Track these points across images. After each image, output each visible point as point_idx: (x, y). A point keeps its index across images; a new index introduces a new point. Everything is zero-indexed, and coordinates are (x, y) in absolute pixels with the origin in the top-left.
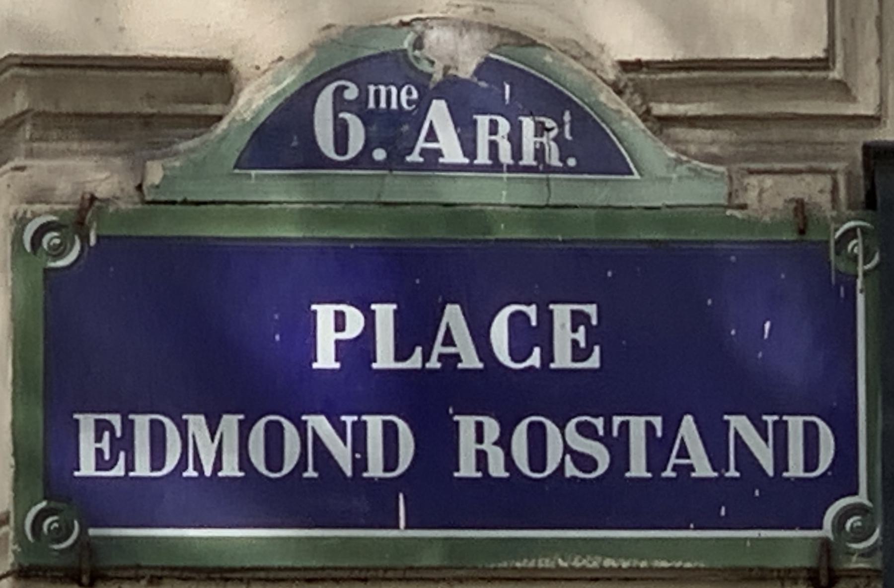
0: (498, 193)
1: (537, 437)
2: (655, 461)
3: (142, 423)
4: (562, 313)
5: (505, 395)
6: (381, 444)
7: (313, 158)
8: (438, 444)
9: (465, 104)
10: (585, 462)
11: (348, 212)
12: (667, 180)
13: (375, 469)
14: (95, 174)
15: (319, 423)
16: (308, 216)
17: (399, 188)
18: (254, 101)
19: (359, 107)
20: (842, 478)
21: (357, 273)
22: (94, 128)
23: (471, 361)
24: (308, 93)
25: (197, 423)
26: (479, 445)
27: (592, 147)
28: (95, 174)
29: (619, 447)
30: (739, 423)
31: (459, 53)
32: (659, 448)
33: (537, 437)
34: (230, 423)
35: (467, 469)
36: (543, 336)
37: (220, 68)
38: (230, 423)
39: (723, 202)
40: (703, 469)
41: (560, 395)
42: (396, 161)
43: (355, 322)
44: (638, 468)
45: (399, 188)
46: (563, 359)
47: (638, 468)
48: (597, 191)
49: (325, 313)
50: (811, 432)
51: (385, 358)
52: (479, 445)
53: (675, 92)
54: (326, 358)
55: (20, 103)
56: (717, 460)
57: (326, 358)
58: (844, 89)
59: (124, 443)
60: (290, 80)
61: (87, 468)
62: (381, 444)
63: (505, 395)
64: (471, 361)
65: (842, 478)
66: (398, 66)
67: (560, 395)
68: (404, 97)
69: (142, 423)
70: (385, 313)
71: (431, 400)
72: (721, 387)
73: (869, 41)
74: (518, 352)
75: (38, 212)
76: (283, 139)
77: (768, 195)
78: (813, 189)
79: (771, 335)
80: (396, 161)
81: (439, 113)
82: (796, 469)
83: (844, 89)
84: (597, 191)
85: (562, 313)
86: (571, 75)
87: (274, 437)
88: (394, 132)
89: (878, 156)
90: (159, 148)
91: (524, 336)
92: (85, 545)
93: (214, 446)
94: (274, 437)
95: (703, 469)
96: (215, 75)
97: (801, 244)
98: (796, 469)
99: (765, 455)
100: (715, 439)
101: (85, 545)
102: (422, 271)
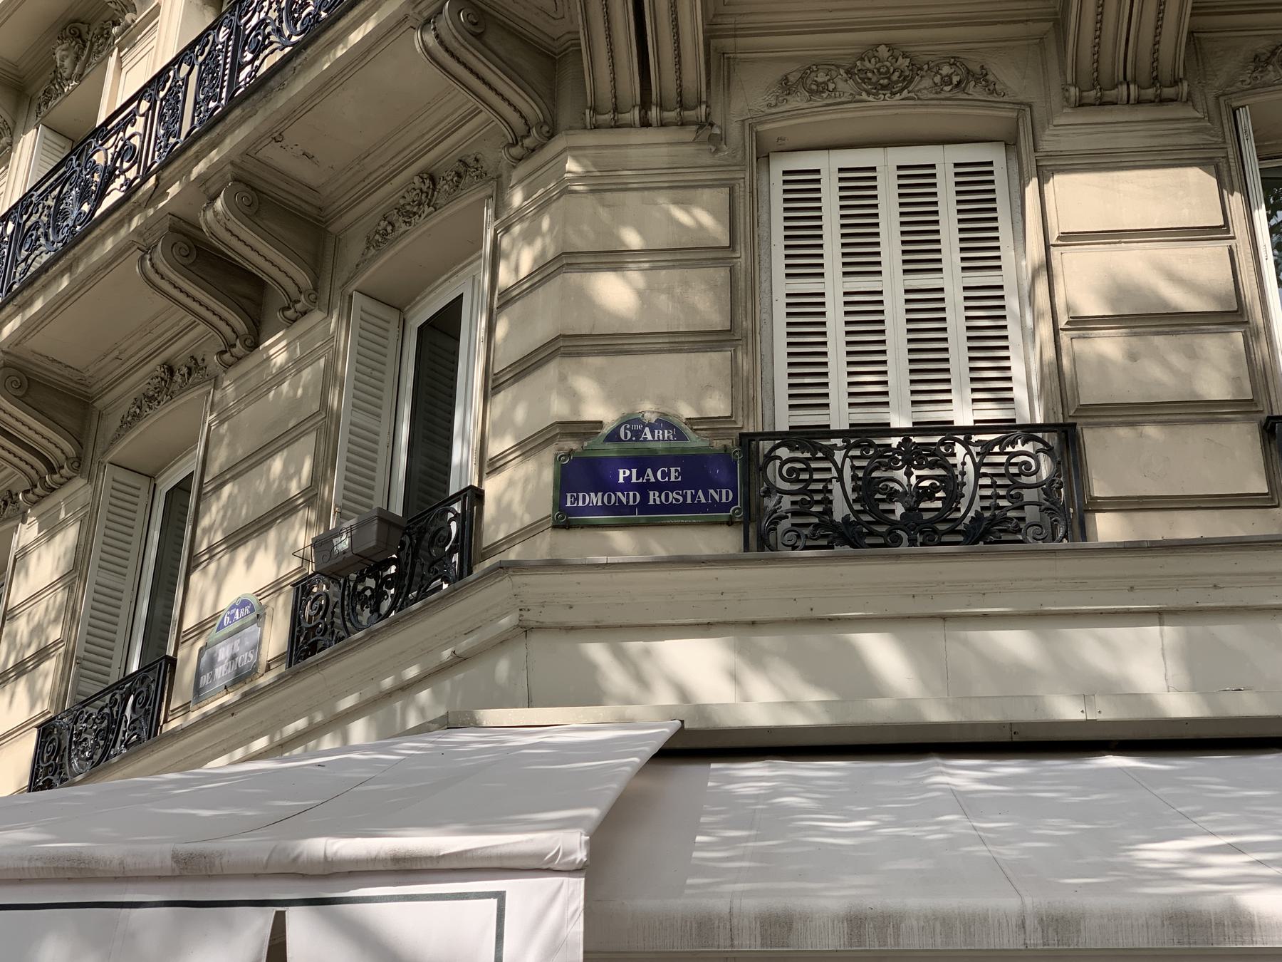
0: (660, 445)
1: (667, 495)
2: (693, 499)
3: (581, 495)
4: (673, 470)
5: (659, 487)
6: (633, 498)
7: (620, 440)
8: (645, 497)
9: (652, 428)
10: (677, 500)
11: (627, 451)
12: (696, 442)
13: (631, 503)
14: (572, 445)
15: (619, 494)
16: (618, 451)
17: (638, 445)
18: (606, 430)
19: (630, 429)
20: (734, 501)
21: (628, 462)
22: (573, 435)
23: (653, 480)
24: (619, 427)
25: (593, 495)
26: (654, 497)
27: (680, 436)
28: (572, 445)
29: (685, 497)
30: (711, 491)
31: (652, 418)
32: (693, 497)
33: (667, 495)
34: (600, 494)
35: (651, 502)
36: (669, 474)
37: (601, 422)
38: (600, 494)
39: (721, 274)
40: (703, 501)
41: (671, 487)
42: (637, 440)
43: (628, 473)
44: (689, 501)
45: (638, 445)
46: (673, 479)
47: (689, 501)
48: (681, 444)
49: (621, 471)
50: (727, 493)
51: (634, 480)
52: (654, 497)
53: (698, 424)
54: (621, 480)
55: (558, 431)
56: (707, 499)
57: (621, 480)
58: (735, 422)
59: (577, 499)
60: (615, 425)
61: (569, 504)
62: (633, 498)
63: (659, 487)
64: (653, 480)
65: (734, 501)
66: (639, 421)
67: (671, 487)
68: (639, 427)
69: (581, 495)
70: (634, 471)
71: (643, 489)
72: (705, 483)
73: (740, 413)
74: (663, 477)
75: (533, 624)
76: (613, 436)
77: (718, 444)
78: (728, 442)
79: (719, 472)
80: (637, 440)
81: (647, 430)
82: (724, 500)
83: (735, 422)
84: (681, 444)
85: (673, 470)
86: (675, 421)
87: (609, 497)
88: (637, 434)
89: (742, 435)
90: (587, 439)
91: (663, 476)
92: (567, 521)
93: (595, 499)
94: (609, 497)
95: (703, 501)
96: (600, 424)
97: (725, 455)
98: (724, 500)
99: (717, 497)
100: (706, 495)
101: (567, 521)
102: (642, 462)
